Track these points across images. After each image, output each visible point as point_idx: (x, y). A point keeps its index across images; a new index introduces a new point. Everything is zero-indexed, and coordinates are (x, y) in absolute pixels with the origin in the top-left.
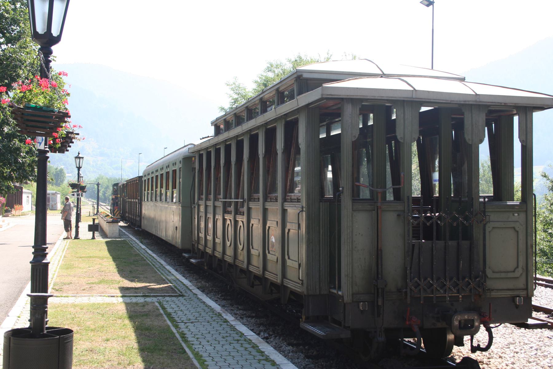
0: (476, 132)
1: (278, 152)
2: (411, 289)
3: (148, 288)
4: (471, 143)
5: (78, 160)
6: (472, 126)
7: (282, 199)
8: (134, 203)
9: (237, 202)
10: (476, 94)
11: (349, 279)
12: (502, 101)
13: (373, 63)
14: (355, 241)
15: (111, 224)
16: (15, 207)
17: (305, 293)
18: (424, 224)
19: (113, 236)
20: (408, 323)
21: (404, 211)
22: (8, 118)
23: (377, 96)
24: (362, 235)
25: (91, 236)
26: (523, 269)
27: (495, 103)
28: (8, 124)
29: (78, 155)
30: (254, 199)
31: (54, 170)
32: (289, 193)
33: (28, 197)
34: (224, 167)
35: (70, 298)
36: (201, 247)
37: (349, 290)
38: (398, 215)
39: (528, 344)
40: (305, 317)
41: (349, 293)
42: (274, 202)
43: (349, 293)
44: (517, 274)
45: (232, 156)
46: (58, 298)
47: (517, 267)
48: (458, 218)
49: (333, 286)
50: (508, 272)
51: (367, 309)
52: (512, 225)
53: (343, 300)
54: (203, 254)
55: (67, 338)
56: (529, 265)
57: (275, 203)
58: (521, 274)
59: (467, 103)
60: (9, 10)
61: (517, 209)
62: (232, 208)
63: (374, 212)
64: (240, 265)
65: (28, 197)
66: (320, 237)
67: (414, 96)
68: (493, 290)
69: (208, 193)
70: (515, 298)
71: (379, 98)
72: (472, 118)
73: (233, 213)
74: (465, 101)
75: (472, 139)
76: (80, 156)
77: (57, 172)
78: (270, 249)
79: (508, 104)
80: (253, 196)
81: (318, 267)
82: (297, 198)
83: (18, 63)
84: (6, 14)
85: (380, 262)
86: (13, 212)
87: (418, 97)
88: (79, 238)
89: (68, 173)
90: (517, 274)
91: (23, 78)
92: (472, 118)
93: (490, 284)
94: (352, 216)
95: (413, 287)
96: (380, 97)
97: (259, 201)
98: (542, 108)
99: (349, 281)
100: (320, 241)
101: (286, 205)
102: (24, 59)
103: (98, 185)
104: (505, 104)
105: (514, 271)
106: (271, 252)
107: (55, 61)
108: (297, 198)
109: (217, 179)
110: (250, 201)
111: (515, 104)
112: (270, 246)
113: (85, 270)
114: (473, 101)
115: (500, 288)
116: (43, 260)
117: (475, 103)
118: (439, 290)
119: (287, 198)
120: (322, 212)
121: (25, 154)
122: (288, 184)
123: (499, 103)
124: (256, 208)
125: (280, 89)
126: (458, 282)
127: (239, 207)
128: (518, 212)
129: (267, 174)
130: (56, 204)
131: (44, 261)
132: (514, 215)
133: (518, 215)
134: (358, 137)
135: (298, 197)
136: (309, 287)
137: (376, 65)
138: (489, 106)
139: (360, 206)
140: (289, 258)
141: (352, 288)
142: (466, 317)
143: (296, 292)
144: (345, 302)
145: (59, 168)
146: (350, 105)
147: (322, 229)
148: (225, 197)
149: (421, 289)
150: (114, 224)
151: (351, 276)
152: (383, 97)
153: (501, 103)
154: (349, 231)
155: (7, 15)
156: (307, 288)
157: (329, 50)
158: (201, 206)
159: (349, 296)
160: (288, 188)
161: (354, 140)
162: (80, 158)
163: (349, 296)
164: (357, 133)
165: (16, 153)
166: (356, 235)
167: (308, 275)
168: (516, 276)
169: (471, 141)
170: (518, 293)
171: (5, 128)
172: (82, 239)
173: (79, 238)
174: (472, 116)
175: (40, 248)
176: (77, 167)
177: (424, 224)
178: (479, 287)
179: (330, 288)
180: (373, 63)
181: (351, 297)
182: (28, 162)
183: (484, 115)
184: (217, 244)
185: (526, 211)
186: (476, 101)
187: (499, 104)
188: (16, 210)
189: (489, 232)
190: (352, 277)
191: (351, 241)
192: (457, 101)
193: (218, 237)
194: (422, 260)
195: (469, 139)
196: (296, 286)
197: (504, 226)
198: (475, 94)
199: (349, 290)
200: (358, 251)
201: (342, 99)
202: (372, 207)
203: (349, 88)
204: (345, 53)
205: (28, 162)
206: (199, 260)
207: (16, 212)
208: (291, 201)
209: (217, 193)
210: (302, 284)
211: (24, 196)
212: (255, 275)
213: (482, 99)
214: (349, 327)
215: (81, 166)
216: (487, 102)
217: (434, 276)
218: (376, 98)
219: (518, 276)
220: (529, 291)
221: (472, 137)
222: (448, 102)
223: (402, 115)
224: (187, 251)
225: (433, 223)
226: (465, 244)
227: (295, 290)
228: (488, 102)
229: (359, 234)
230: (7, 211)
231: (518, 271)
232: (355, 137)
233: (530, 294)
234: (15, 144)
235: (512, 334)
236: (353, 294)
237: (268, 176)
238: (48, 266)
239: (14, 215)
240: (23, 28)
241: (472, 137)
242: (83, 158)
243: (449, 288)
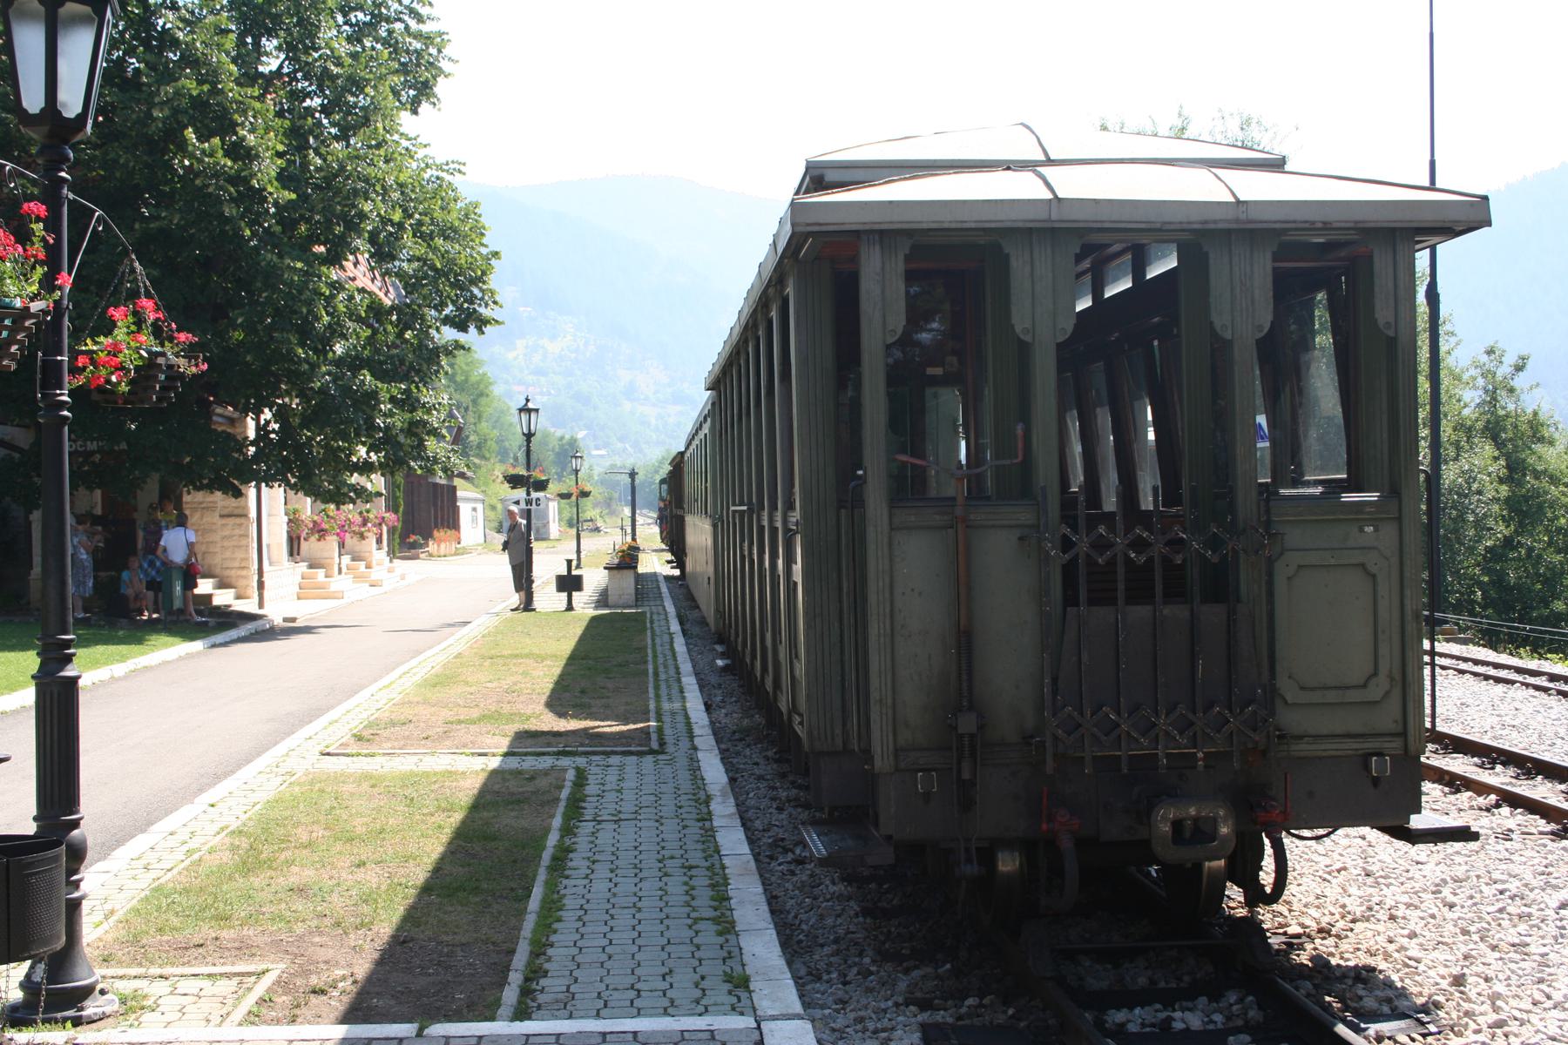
0: (1244, 305)
2: (1056, 738)
3: (588, 734)
4: (1230, 337)
5: (524, 417)
8: (449, 522)
10: (1238, 202)
11: (884, 711)
12: (1317, 216)
13: (1033, 133)
14: (900, 611)
15: (615, 572)
16: (436, 533)
18: (1166, 560)
19: (621, 602)
20: (1044, 826)
22: (344, 321)
23: (947, 220)
25: (564, 605)
26: (1392, 679)
27: (1294, 222)
28: (344, 337)
29: (526, 405)
31: (556, 443)
33: (474, 509)
35: (378, 759)
37: (885, 738)
39: (1501, 881)
41: (885, 749)
43: (885, 749)
44: (1375, 692)
46: (351, 758)
47: (1375, 674)
50: (1348, 688)
51: (935, 790)
55: (33, 863)
56: (1409, 668)
58: (1387, 694)
59: (1212, 226)
60: (340, 57)
61: (1369, 513)
63: (950, 530)
65: (474, 509)
66: (840, 601)
67: (1054, 217)
68: (1301, 737)
71: (954, 226)
74: (1206, 222)
76: (530, 405)
77: (563, 445)
79: (1335, 225)
81: (839, 678)
83: (361, 185)
84: (333, 68)
86: (432, 547)
87: (1065, 218)
88: (534, 610)
89: (597, 448)
90: (1375, 692)
91: (373, 220)
96: (957, 222)
98: (1451, 230)
99: (884, 717)
102: (373, 175)
103: (633, 475)
104: (1324, 223)
105: (1364, 686)
107: (464, 174)
111: (1356, 222)
113: (472, 689)
115: (1325, 732)
116: (62, 670)
117: (1234, 226)
118: (1137, 740)
121: (389, 406)
123: (1306, 222)
126: (1191, 716)
128: (1374, 522)
130: (546, 525)
131: (63, 674)
132: (1361, 530)
133: (1376, 530)
134: (904, 332)
137: (1037, 137)
138: (1284, 231)
139: (913, 518)
141: (895, 734)
142: (1192, 811)
145: (567, 437)
146: (877, 248)
149: (1122, 736)
150: (621, 571)
151: (890, 701)
152: (965, 222)
153: (1313, 223)
154: (881, 584)
155: (335, 70)
157: (1181, 107)
161: (1061, 339)
162: (529, 411)
164: (1069, 326)
165: (369, 405)
169: (1230, 332)
170: (1377, 745)
171: (338, 345)
172: (542, 610)
173: (534, 610)
175: (51, 641)
176: (524, 434)
177: (1166, 560)
178: (1255, 730)
180: (1033, 133)
181: (891, 758)
182: (399, 424)
183: (1269, 256)
185: (1399, 519)
186: (1237, 221)
187: (1307, 225)
188: (439, 542)
189: (1289, 578)
191: (888, 610)
192: (1181, 223)
194: (1085, 657)
197: (1333, 562)
198: (1233, 200)
199: (885, 738)
200: (910, 636)
201: (857, 233)
202: (946, 518)
203: (1002, 201)
204: (1220, 110)
205: (399, 424)
207: (439, 546)
211: (465, 510)
213: (1253, 215)
215: (533, 431)
216: (1270, 222)
218: (946, 225)
220: (1411, 739)
222: (1153, 226)
225: (1077, 555)
226: (1212, 615)
228: (1275, 222)
230: (414, 546)
231: (1377, 686)
232: (1262, 331)
233: (1412, 748)
234: (363, 382)
235: (1477, 852)
236: (897, 751)
238: (77, 682)
239: (431, 555)
240: (372, 98)
242: (537, 410)
243: (1167, 733)
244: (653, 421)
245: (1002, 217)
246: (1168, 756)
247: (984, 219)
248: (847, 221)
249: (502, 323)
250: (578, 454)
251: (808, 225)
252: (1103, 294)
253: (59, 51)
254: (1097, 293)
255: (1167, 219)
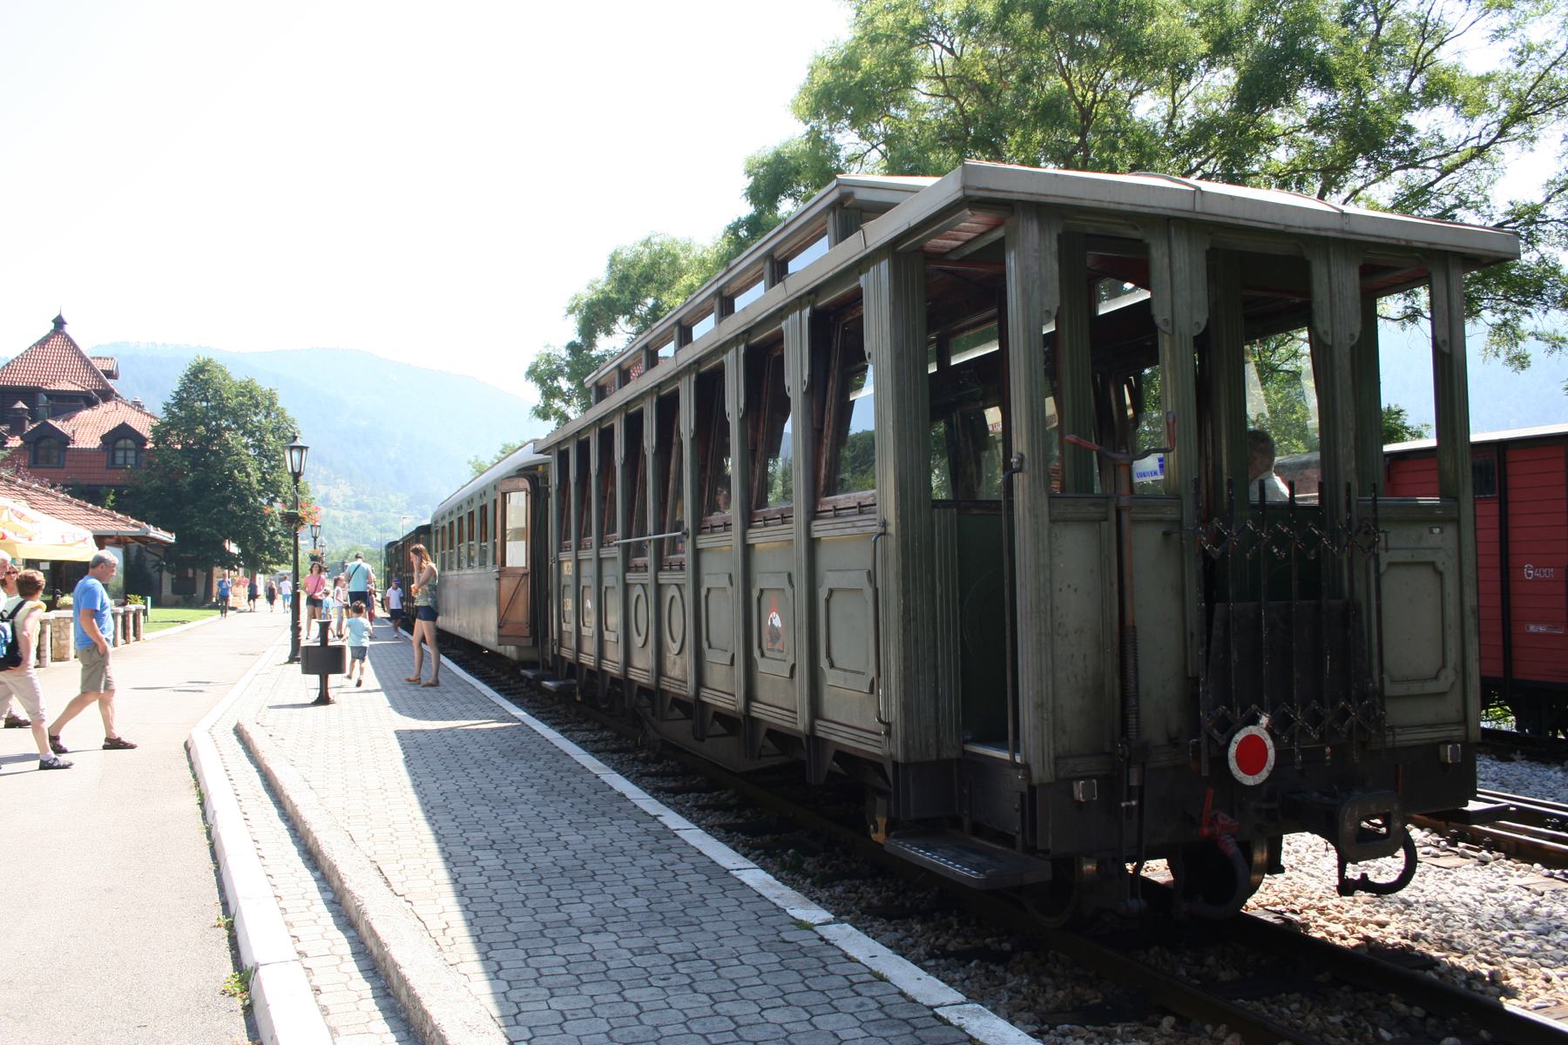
1: (790, 394)
2: (1210, 737)
6: (1331, 297)
7: (808, 513)
9: (662, 540)
17: (900, 758)
21: (1180, 522)
24: (1076, 590)
26: (1455, 669)
27: (1385, 237)
30: (713, 527)
32: (827, 496)
34: (623, 466)
36: (567, 654)
38: (1166, 534)
40: (885, 820)
42: (676, 570)
45: (647, 436)
47: (1444, 666)
48: (1319, 538)
49: (969, 737)
52: (1430, 557)
53: (1028, 775)
54: (574, 668)
57: (781, 527)
58: (1453, 684)
62: (649, 559)
63: (1104, 524)
64: (672, 690)
66: (934, 604)
67: (1198, 208)
69: (583, 531)
70: (1442, 749)
72: (1330, 278)
73: (651, 569)
75: (1332, 332)
78: (765, 646)
80: (706, 521)
82: (859, 503)
85: (1131, 661)
87: (1207, 210)
92: (1330, 278)
93: (1395, 714)
94: (1049, 536)
95: (1216, 732)
97: (646, 571)
100: (935, 617)
101: (817, 528)
105: (1436, 678)
106: (767, 653)
108: (859, 503)
109: (606, 498)
110: (700, 533)
111: (1430, 244)
112: (766, 637)
114: (1335, 230)
117: (1340, 235)
119: (819, 509)
120: (940, 535)
122: (823, 472)
123: (1393, 238)
124: (721, 549)
125: (776, 255)
127: (665, 553)
129: (750, 461)
132: (1431, 532)
133: (1442, 532)
135: (861, 500)
136: (911, 742)
140: (832, 666)
141: (1055, 742)
143: (859, 754)
144: (1035, 781)
146: (1035, 224)
147: (941, 584)
148: (627, 535)
154: (1042, 579)
156: (905, 744)
158: (565, 565)
159: (1046, 767)
160: (822, 483)
163: (1046, 767)
166: (1060, 590)
167: (906, 707)
168: (1440, 690)
169: (1330, 338)
174: (1329, 272)
179: (966, 742)
181: (1052, 767)
184: (609, 643)
190: (1054, 708)
191: (1049, 607)
192: (1300, 227)
193: (610, 628)
195: (1326, 332)
196: (861, 740)
200: (1066, 635)
206: (562, 683)
208: (836, 516)
209: (606, 527)
210: (888, 733)
212: (716, 713)
214: (1047, 852)
217: (1265, 697)
219: (1446, 690)
221: (1332, 326)
223: (1166, 260)
224: (531, 665)
227: (856, 749)
228: (1370, 236)
229: (1069, 586)
236: (1057, 758)
237: (754, 464)
241: (1332, 326)
244: (342, 522)
245: (1153, 203)
246: (1303, 751)
247: (1138, 203)
248: (1015, 190)
249: (132, 747)
250: (317, 524)
251: (979, 189)
252: (949, 361)
253: (466, 637)
254: (943, 361)
255: (1289, 223)
